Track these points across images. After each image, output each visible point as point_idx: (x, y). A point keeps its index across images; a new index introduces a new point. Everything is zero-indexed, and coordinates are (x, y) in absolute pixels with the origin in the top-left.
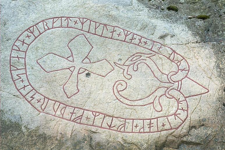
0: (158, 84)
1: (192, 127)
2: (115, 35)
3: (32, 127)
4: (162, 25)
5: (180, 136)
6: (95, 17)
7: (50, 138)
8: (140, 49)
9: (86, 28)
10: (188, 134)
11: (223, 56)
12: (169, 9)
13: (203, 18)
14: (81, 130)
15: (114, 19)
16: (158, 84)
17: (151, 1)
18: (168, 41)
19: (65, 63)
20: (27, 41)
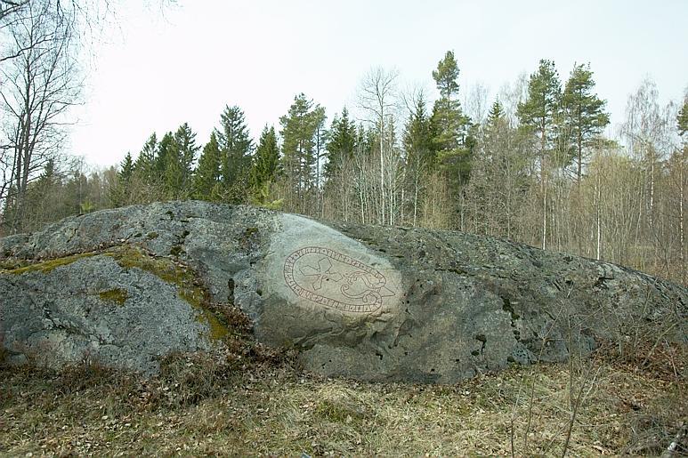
0: (366, 288)
1: (382, 312)
2: (346, 261)
3: (293, 302)
4: (374, 258)
5: (375, 316)
6: (336, 250)
7: (303, 309)
8: (360, 270)
9: (329, 255)
10: (380, 316)
11: (685, 416)
12: (380, 250)
13: (399, 257)
14: (321, 307)
15: (347, 252)
16: (366, 288)
17: (62, 451)
18: (376, 266)
19: (315, 272)
20: (295, 258)
